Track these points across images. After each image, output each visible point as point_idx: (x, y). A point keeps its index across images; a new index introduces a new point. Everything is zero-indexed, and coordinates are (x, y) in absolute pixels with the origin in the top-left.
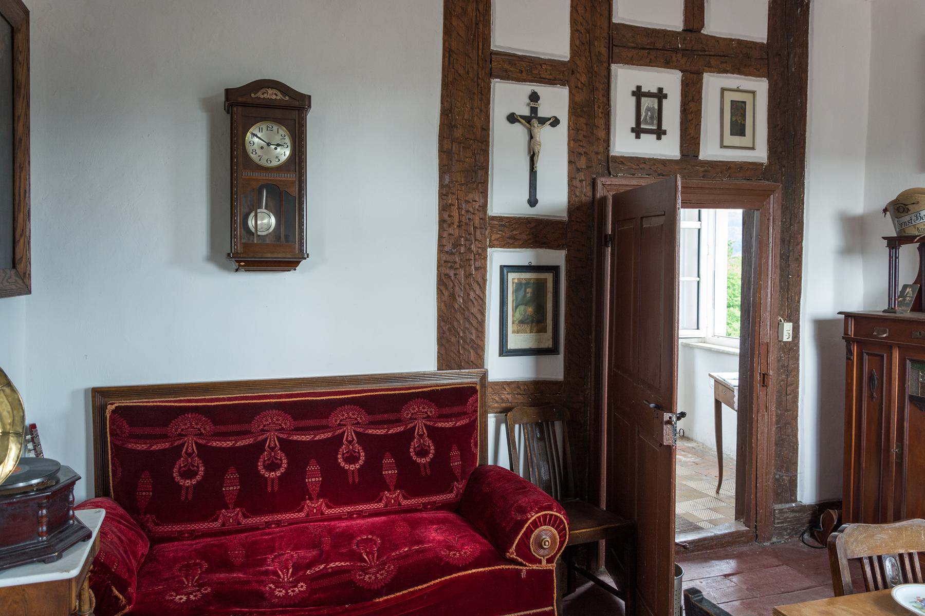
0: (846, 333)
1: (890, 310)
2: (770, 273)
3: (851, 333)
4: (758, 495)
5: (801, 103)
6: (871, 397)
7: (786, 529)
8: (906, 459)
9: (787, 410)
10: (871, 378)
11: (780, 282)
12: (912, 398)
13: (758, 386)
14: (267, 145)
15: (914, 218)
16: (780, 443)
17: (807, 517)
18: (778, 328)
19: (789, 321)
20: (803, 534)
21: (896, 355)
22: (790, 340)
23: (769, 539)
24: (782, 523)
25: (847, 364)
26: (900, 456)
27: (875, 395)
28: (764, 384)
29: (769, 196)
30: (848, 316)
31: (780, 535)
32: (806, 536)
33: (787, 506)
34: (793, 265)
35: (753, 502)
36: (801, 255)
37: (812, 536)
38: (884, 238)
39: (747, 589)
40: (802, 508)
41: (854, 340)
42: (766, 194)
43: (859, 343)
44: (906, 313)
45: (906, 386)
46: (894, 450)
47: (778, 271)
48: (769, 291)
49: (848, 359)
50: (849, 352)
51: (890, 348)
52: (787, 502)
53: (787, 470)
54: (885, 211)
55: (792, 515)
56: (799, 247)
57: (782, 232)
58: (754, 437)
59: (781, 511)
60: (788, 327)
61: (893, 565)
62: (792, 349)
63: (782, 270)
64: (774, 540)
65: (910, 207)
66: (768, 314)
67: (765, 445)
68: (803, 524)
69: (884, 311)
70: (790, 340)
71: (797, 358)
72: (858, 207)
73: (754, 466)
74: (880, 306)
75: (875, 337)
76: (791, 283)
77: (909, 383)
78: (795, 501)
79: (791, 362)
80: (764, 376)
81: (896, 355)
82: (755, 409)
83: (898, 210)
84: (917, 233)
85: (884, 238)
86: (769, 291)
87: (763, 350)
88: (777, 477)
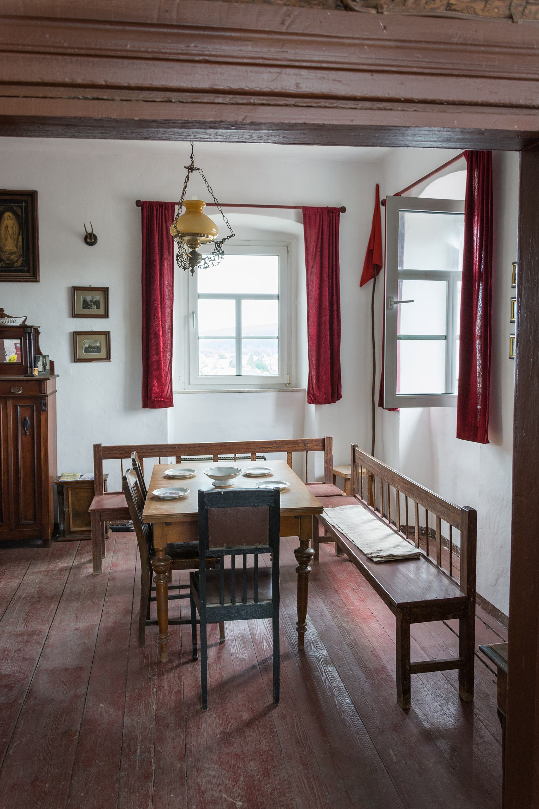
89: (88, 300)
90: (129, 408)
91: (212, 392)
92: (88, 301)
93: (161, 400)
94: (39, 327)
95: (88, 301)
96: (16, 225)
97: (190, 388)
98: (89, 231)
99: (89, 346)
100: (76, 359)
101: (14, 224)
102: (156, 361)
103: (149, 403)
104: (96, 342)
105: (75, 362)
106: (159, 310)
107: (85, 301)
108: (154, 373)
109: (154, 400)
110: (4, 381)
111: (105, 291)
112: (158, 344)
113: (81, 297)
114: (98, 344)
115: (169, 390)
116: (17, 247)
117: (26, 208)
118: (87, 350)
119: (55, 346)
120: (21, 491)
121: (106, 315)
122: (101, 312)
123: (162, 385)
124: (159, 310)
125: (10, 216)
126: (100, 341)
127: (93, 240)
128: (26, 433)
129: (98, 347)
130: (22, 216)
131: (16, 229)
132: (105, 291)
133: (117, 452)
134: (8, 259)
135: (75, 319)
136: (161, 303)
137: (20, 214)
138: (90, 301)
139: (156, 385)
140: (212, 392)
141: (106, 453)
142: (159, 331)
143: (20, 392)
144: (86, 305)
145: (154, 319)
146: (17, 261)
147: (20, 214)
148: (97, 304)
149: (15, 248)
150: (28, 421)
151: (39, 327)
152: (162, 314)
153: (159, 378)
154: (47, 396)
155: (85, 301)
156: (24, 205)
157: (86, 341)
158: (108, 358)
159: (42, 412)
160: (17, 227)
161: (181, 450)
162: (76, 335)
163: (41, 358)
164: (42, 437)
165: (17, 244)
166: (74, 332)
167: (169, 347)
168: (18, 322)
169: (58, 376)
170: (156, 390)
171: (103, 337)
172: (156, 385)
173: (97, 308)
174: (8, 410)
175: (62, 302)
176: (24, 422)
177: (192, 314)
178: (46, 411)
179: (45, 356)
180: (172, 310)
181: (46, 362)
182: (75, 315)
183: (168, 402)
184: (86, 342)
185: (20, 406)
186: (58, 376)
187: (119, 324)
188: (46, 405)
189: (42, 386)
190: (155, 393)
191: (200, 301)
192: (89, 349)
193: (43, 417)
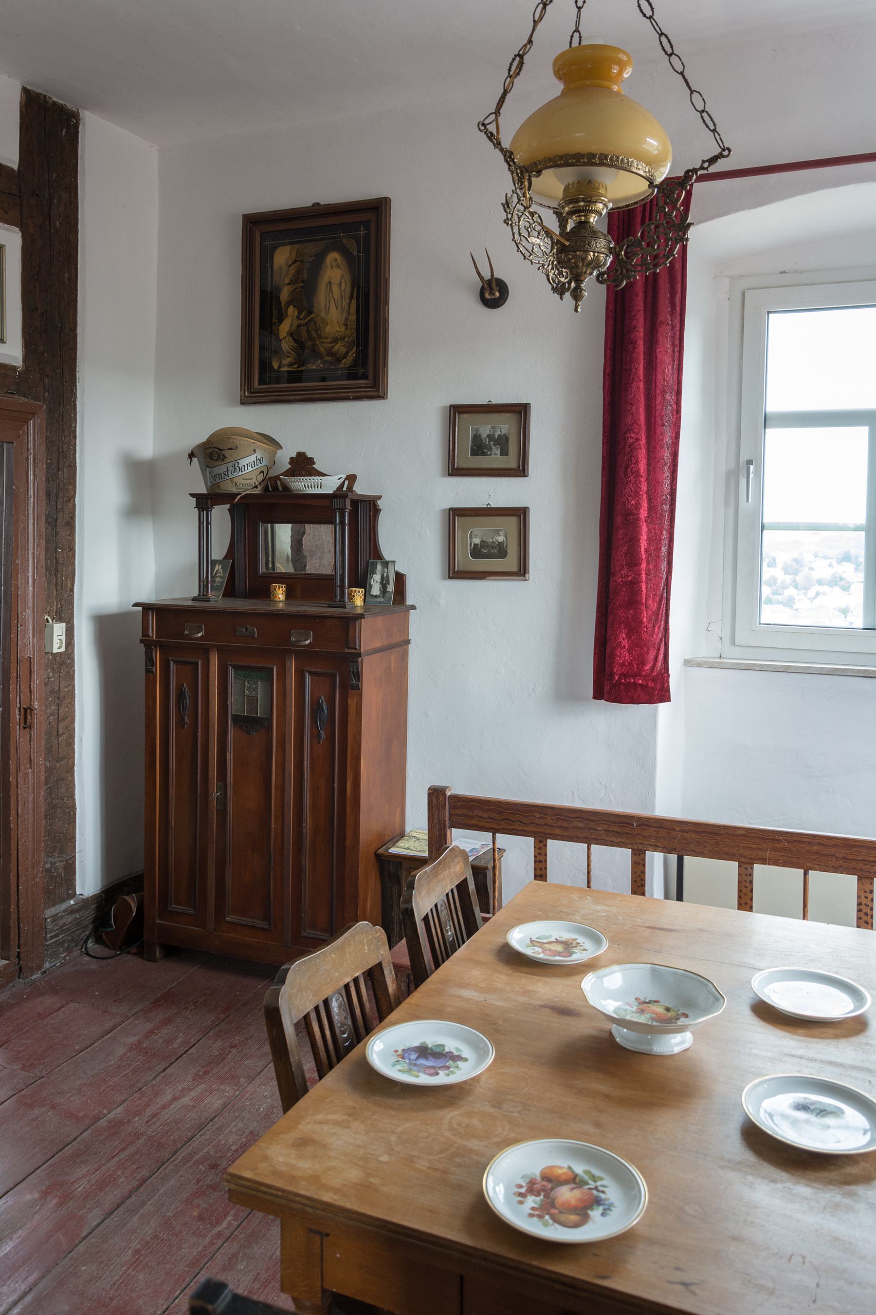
0: (145, 633)
1: (202, 597)
2: (31, 545)
3: (153, 633)
4: (21, 902)
5: (69, 279)
6: (181, 722)
7: (61, 944)
8: (230, 805)
9: (59, 760)
10: (180, 696)
11: (46, 559)
12: (237, 719)
13: (16, 729)
14: (539, 873)
15: (231, 468)
16: (49, 815)
17: (89, 914)
18: (42, 632)
19: (60, 620)
20: (86, 941)
21: (214, 661)
22: (63, 649)
23: (39, 967)
24: (56, 935)
25: (147, 678)
26: (223, 800)
27: (186, 720)
28: (27, 725)
29: (27, 422)
30: (147, 608)
31: (55, 955)
32: (90, 944)
33: (63, 906)
34: (63, 533)
35: (14, 917)
36: (73, 518)
37: (99, 940)
38: (192, 495)
39: (23, 1068)
40: (85, 903)
41: (156, 644)
42: (22, 418)
43: (163, 647)
44: (217, 600)
45: (229, 703)
46: (215, 794)
47: (43, 542)
48: (30, 574)
49: (148, 671)
50: (150, 661)
51: (205, 652)
52: (63, 900)
53: (62, 852)
54: (191, 455)
55: (70, 919)
56: (70, 504)
57: (47, 480)
58: (13, 812)
59: (55, 918)
60: (59, 629)
61: (340, 1007)
62: (65, 663)
63: (48, 541)
64: (47, 965)
65: (227, 453)
66: (30, 612)
67: (31, 821)
68: (86, 927)
69: (194, 599)
70: (63, 649)
71: (71, 677)
72: (147, 448)
73: (14, 855)
74: (184, 591)
75: (187, 637)
76: (61, 560)
77: (232, 699)
78: (74, 894)
79: (63, 684)
80: (27, 712)
81: (214, 661)
82: (13, 768)
83: (210, 456)
84: (234, 490)
85: (192, 495)
86: (30, 574)
87: (23, 671)
88: (48, 866)
89: (484, 436)
90: (563, 696)
91: (787, 670)
92: (487, 437)
93: (635, 684)
94: (380, 497)
95: (487, 437)
96: (348, 278)
97: (733, 655)
98: (487, 275)
99: (483, 542)
100: (455, 573)
101: (342, 276)
102: (626, 583)
103: (607, 688)
104: (497, 532)
105: (450, 578)
106: (642, 453)
107: (476, 438)
108: (621, 613)
109: (619, 683)
110: (258, 614)
111: (521, 411)
112: (634, 541)
113: (470, 426)
114: (501, 539)
115: (661, 657)
116: (346, 325)
117: (367, 236)
118: (477, 552)
119: (410, 542)
120: (306, 862)
121: (521, 471)
122: (511, 462)
123: (639, 645)
124: (642, 453)
125: (336, 260)
126: (503, 533)
127: (497, 294)
128: (319, 734)
129: (500, 544)
130: (359, 257)
131: (346, 287)
132: (521, 411)
133: (485, 815)
134: (330, 353)
135: (455, 480)
136: (648, 438)
137: (355, 253)
138: (489, 436)
139: (625, 643)
140: (787, 670)
141: (458, 812)
142: (638, 506)
143: (307, 642)
144: (479, 448)
145: (626, 476)
146: (345, 355)
147: (355, 253)
148: (502, 442)
149: (343, 329)
150: (325, 708)
151: (380, 497)
152: (649, 465)
153: (634, 627)
154: (359, 655)
155: (476, 438)
156: (362, 232)
157: (476, 530)
158: (522, 571)
159: (350, 690)
160: (349, 283)
161: (645, 833)
162: (455, 514)
163: (379, 567)
164: (349, 749)
165: (347, 319)
166: (450, 509)
167: (664, 549)
168: (329, 485)
169: (413, 607)
170: (623, 656)
171: (513, 521)
172: (625, 643)
173: (502, 454)
174: (287, 680)
175: (429, 439)
176: (316, 709)
177: (741, 470)
178: (358, 688)
179: (387, 562)
180: (675, 455)
181: (388, 576)
182: (454, 471)
183: (656, 690)
184: (477, 533)
185: (310, 673)
186: (413, 607)
187: (551, 491)
188: (358, 676)
189: (351, 633)
190: (622, 665)
191: (772, 434)
192: (486, 549)
193: (352, 703)
